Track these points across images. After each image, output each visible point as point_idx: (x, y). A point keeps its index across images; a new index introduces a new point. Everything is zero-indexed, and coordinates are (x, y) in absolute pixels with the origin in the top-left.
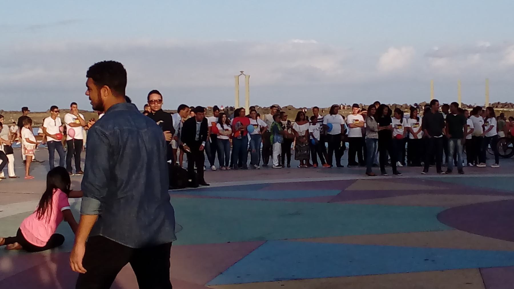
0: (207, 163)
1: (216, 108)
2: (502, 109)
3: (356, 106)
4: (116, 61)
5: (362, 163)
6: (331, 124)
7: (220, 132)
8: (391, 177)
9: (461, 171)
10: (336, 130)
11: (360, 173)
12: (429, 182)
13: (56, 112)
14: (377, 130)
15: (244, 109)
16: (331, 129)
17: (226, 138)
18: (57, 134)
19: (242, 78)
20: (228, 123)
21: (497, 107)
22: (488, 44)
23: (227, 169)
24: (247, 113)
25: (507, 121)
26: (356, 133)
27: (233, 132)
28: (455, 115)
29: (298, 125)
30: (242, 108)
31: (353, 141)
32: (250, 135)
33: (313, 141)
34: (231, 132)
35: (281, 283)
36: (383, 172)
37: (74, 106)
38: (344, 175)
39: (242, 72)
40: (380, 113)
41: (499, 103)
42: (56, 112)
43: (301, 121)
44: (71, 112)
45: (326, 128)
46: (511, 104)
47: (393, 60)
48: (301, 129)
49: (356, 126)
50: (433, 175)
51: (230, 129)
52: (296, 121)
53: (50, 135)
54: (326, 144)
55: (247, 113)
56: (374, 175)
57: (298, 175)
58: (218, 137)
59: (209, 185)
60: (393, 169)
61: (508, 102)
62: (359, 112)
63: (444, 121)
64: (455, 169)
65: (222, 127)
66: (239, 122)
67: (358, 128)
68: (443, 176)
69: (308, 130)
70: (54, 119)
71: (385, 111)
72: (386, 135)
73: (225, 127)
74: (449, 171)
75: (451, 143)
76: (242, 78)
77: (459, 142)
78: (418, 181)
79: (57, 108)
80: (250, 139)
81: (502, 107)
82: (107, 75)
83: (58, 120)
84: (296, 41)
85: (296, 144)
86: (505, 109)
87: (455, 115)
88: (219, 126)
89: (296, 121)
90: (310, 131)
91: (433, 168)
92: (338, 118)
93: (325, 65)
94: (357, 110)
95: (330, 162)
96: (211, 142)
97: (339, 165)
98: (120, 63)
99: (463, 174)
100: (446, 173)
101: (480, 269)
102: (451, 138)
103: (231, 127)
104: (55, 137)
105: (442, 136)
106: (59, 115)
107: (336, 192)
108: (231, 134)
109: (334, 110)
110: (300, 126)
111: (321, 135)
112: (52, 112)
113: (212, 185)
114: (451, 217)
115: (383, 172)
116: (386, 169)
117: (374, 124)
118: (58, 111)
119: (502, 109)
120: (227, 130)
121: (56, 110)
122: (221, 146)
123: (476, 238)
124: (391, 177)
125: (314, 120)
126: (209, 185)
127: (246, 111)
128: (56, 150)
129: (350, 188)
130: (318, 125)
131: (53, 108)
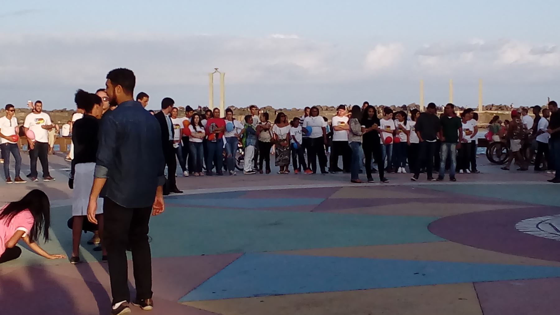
0: (179, 168)
1: (189, 109)
2: (496, 112)
3: (342, 107)
4: (123, 67)
5: (347, 169)
6: (311, 128)
7: (193, 134)
8: (378, 184)
9: (452, 179)
10: (317, 133)
11: (345, 180)
12: (418, 190)
13: (12, 111)
14: (361, 133)
15: (219, 110)
16: (311, 131)
17: (199, 141)
18: (13, 136)
19: (217, 76)
20: (201, 125)
21: (491, 109)
22: (482, 42)
23: (200, 175)
24: (222, 115)
25: (503, 124)
26: (341, 136)
27: (206, 135)
28: (450, 117)
29: (278, 128)
30: (148, 97)
32: (226, 138)
33: (295, 144)
34: (204, 134)
35: (260, 299)
36: (370, 179)
37: (38, 104)
39: (216, 69)
40: (365, 115)
41: (493, 105)
42: (12, 111)
43: (282, 124)
44: (36, 111)
45: (306, 131)
46: (505, 106)
48: (282, 131)
49: (341, 129)
50: (423, 182)
51: (203, 131)
52: (275, 123)
53: (4, 137)
55: (222, 115)
56: (360, 183)
57: (277, 182)
58: (190, 140)
59: (182, 192)
60: (380, 176)
61: (503, 105)
62: (344, 115)
63: (439, 123)
64: (447, 176)
65: (195, 128)
66: (214, 124)
67: (344, 131)
68: (434, 183)
69: (289, 133)
70: (10, 119)
71: (371, 112)
72: (372, 139)
73: (198, 128)
74: (441, 178)
75: (444, 147)
76: (217, 76)
77: (453, 147)
78: (408, 188)
79: (12, 106)
80: (225, 142)
81: (496, 110)
83: (14, 121)
84: (276, 36)
85: (276, 149)
86: (499, 112)
87: (450, 117)
88: (191, 127)
89: (275, 123)
90: (291, 134)
91: (423, 175)
92: (319, 119)
93: (307, 62)
94: (342, 111)
96: (183, 145)
97: (323, 171)
98: (131, 71)
99: (455, 181)
100: (437, 180)
101: (473, 283)
102: (444, 142)
103: (205, 129)
104: (11, 138)
105: (435, 141)
106: (14, 115)
107: (318, 201)
108: (205, 137)
110: (281, 129)
111: (303, 138)
112: (7, 111)
113: (186, 192)
114: (442, 228)
115: (370, 179)
116: (373, 175)
117: (358, 127)
118: (14, 110)
119: (496, 112)
120: (200, 132)
121: (11, 109)
122: (194, 151)
123: (471, 251)
124: (378, 184)
125: (295, 123)
126: (182, 192)
127: (221, 112)
128: (11, 153)
129: (335, 196)
130: (299, 128)
131: (8, 107)
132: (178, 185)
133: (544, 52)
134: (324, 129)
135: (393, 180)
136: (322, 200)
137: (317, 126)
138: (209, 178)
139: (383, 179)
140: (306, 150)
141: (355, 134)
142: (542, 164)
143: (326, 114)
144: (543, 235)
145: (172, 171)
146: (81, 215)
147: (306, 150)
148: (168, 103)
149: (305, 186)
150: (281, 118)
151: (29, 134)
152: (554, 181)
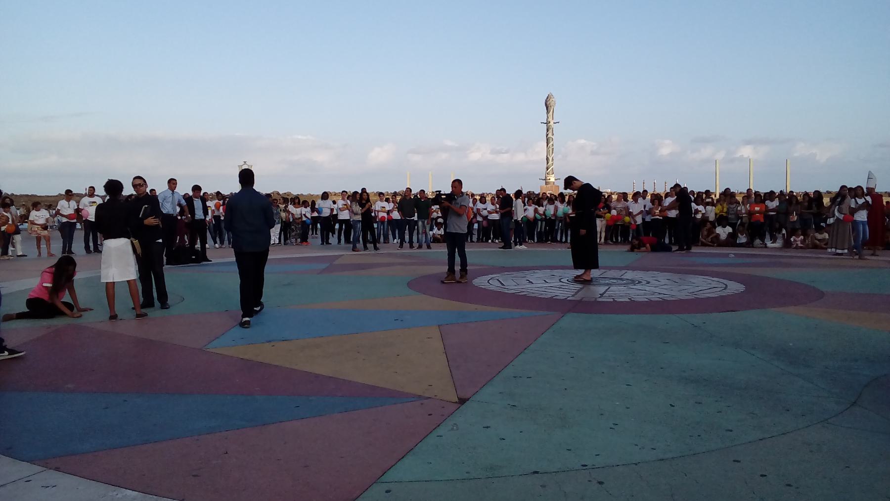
1: (218, 193)
9: (429, 247)
10: (326, 213)
11: (346, 249)
12: (403, 256)
26: (345, 215)
31: (342, 222)
35: (272, 344)
36: (366, 248)
38: (337, 250)
40: (361, 198)
47: (379, 156)
54: (667, 241)
72: (368, 218)
74: (420, 247)
82: (247, 177)
92: (328, 203)
93: (321, 157)
95: (402, 240)
109: (325, 196)
113: (214, 261)
115: (366, 248)
117: (357, 208)
129: (337, 262)
131: (69, 192)
132: (209, 254)
133: (499, 152)
134: (332, 210)
135: (384, 249)
136: (327, 265)
137: (326, 208)
138: (286, 247)
139: (376, 248)
140: (319, 225)
141: (356, 214)
142: (146, 222)
143: (335, 198)
144: (492, 288)
145: (203, 243)
146: (236, 268)
147: (319, 225)
148: (197, 189)
149: (314, 255)
150: (297, 201)
151: (83, 213)
152: (502, 248)
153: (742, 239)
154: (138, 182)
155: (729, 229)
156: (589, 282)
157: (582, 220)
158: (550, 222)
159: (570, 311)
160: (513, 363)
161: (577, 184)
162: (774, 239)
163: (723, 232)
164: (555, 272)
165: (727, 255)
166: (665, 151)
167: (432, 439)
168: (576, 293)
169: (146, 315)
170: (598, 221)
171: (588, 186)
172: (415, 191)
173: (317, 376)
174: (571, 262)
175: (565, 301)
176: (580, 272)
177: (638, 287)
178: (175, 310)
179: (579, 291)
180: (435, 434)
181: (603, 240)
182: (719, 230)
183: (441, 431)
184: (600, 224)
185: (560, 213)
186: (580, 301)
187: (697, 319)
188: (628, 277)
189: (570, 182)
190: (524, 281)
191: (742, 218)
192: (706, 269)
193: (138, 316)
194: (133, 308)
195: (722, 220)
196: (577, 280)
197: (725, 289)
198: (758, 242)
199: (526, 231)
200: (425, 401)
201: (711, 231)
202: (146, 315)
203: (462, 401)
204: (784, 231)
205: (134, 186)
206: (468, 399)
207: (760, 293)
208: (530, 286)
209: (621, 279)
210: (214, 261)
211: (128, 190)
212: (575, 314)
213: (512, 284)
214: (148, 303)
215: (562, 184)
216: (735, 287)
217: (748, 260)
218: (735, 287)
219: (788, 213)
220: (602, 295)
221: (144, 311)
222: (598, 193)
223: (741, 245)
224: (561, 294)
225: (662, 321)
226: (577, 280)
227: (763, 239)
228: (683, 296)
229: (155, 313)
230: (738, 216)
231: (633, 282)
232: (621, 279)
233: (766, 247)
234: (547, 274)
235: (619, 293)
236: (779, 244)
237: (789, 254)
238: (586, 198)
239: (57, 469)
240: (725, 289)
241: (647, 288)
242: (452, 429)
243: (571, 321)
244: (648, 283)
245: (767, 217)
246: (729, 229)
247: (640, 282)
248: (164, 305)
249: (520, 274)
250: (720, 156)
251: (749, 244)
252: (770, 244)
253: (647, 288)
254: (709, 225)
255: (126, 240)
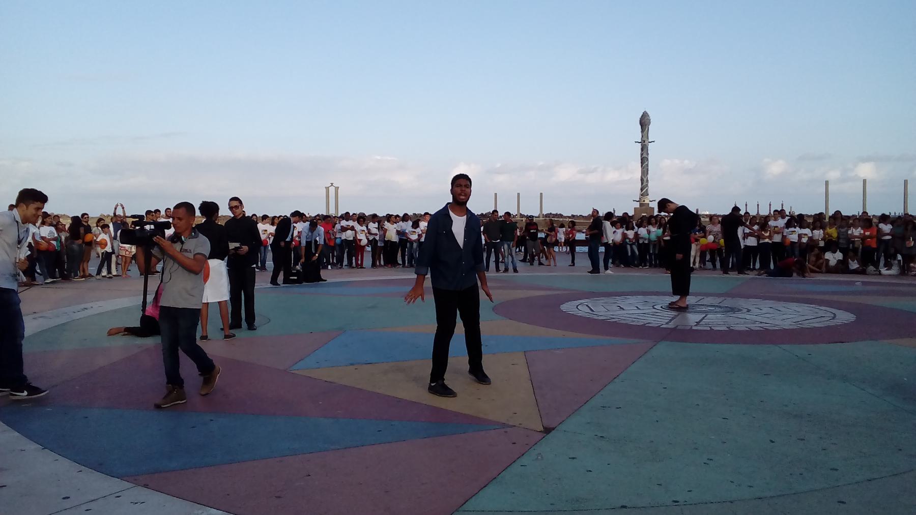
35: (356, 367)
93: (404, 179)
113: (329, 280)
144: (580, 314)
153: (854, 265)
154: (235, 203)
155: (839, 256)
156: (682, 309)
157: (672, 243)
158: (644, 247)
159: (664, 339)
160: (602, 393)
161: (672, 207)
162: (888, 266)
163: (833, 258)
164: (648, 298)
165: (852, 283)
166: (776, 168)
167: (516, 468)
168: (671, 321)
169: (234, 336)
170: (694, 246)
171: (683, 209)
172: (501, 213)
173: (400, 400)
174: (670, 289)
175: (658, 329)
176: (676, 298)
177: (740, 315)
178: (263, 329)
179: (673, 318)
180: (519, 462)
181: (697, 265)
182: (828, 255)
183: (524, 460)
184: (694, 250)
185: (653, 237)
186: (674, 330)
187: (800, 350)
188: (723, 303)
189: (664, 204)
190: (615, 307)
191: (853, 242)
192: (810, 296)
193: (226, 337)
194: (222, 329)
195: (831, 245)
196: (672, 306)
197: (834, 318)
198: (871, 268)
199: (620, 255)
200: (508, 429)
201: (819, 257)
202: (234, 336)
203: (547, 430)
204: (899, 257)
205: (231, 208)
206: (553, 429)
207: (871, 324)
208: (622, 312)
209: (720, 307)
210: (329, 280)
211: (225, 212)
212: (668, 342)
213: (603, 310)
214: (236, 324)
215: (655, 205)
216: (844, 317)
217: (875, 288)
218: (844, 317)
219: (904, 238)
220: (698, 323)
221: (231, 331)
222: (695, 217)
223: (855, 272)
224: (654, 321)
225: (765, 352)
226: (672, 306)
227: (876, 265)
228: (787, 325)
229: (242, 334)
230: (850, 240)
231: (733, 310)
232: (720, 307)
233: (880, 274)
234: (641, 300)
235: (717, 321)
236: (894, 271)
237: (905, 282)
238: (682, 221)
239: (146, 486)
240: (834, 318)
241: (748, 317)
242: (537, 459)
243: (664, 349)
244: (749, 311)
245: (880, 241)
246: (839, 256)
247: (739, 310)
248: (251, 326)
249: (611, 300)
250: (833, 175)
251: (861, 272)
252: (884, 271)
253: (748, 317)
254: (816, 251)
255: (220, 261)
